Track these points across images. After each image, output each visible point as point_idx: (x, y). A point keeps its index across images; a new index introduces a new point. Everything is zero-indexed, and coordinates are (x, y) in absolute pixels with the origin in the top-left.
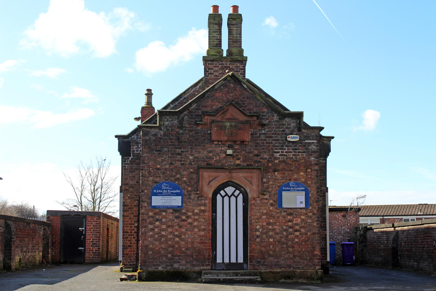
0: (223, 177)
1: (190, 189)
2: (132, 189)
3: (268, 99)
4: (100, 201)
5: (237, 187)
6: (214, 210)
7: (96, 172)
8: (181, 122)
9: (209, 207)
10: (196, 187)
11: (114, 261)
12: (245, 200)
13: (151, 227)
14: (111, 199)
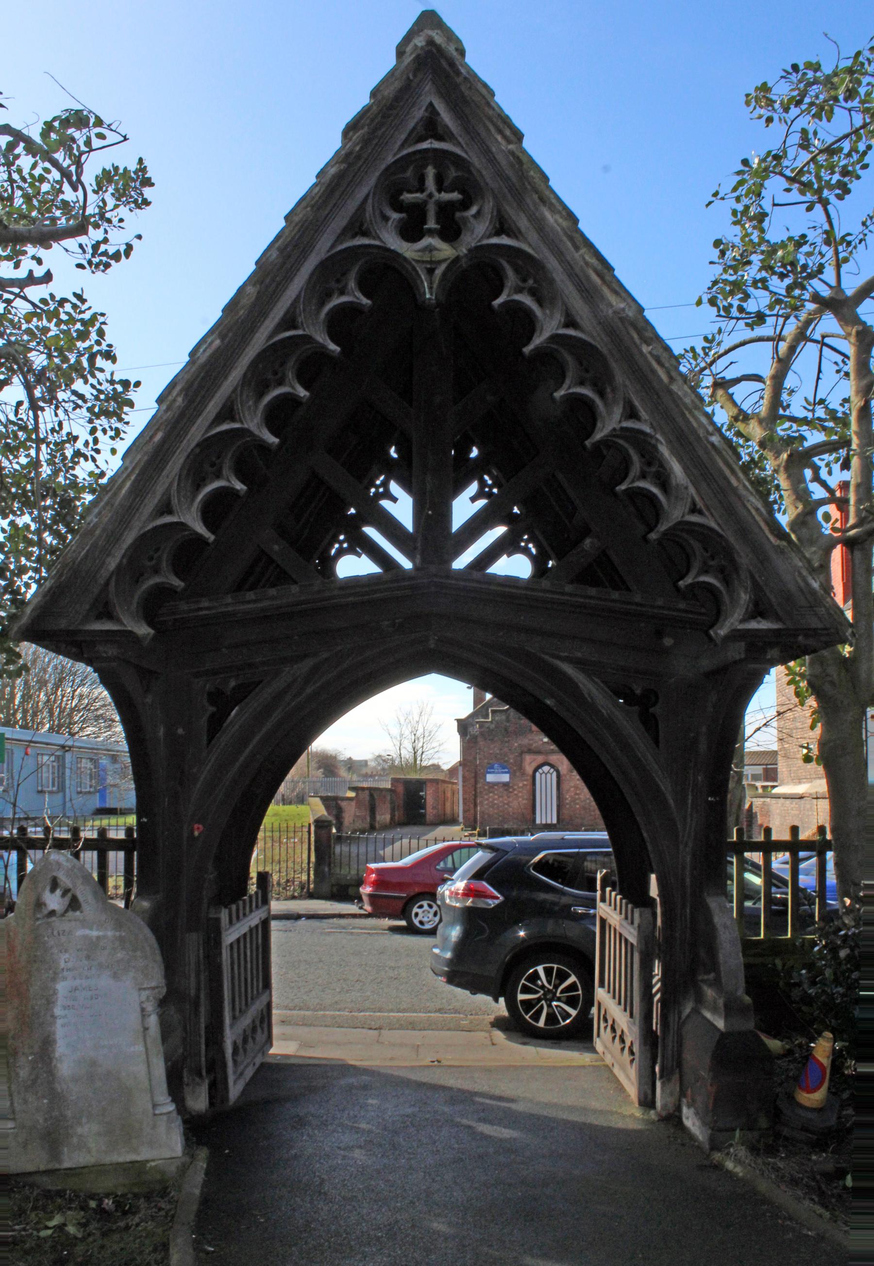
0: (540, 759)
1: (516, 769)
2: (471, 764)
6: (534, 784)
7: (416, 718)
9: (527, 783)
10: (520, 766)
11: (453, 821)
12: (559, 776)
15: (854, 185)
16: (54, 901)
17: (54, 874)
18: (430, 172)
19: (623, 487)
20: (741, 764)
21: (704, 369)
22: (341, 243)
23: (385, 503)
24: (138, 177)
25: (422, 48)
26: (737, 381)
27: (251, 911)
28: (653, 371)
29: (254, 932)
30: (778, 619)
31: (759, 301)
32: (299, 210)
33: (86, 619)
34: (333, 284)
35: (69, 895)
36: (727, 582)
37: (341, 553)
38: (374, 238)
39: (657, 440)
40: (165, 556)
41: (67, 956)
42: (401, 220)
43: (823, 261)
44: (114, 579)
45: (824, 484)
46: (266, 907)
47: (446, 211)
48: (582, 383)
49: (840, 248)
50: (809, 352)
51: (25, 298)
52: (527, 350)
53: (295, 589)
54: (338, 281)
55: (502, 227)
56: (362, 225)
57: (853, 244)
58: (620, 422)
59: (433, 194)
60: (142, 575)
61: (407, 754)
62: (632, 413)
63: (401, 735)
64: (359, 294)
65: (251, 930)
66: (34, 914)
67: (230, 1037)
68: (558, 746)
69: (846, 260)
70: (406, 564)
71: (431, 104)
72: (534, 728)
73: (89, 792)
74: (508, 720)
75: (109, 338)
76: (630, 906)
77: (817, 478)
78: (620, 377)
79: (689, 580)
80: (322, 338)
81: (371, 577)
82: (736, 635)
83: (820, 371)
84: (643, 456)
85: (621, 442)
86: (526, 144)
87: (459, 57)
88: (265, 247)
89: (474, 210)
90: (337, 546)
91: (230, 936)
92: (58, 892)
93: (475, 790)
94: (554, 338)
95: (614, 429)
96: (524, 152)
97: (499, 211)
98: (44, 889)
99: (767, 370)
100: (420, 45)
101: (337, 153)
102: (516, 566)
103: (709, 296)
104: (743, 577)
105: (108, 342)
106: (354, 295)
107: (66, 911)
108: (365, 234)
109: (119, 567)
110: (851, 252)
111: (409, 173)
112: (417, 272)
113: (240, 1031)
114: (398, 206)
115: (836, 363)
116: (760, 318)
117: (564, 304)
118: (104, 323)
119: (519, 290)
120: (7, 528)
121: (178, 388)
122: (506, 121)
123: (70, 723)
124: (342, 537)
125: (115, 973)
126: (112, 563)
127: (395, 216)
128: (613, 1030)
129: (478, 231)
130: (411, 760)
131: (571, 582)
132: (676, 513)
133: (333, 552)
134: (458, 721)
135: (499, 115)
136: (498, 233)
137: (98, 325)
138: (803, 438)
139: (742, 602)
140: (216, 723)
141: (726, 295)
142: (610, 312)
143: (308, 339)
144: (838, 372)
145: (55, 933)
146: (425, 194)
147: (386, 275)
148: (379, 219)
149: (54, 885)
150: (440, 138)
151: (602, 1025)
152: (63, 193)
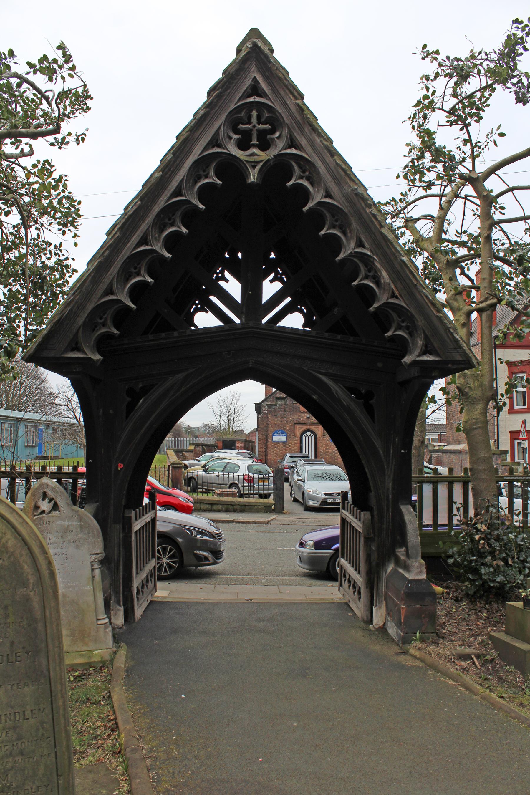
0: (305, 427)
1: (290, 434)
3: (406, 269)
4: (234, 423)
5: (312, 432)
8: (286, 402)
9: (298, 442)
10: (293, 431)
12: (316, 438)
13: (272, 450)
14: (242, 421)
15: (482, 114)
16: (45, 506)
17: (45, 490)
18: (254, 113)
19: (355, 283)
20: (423, 432)
21: (401, 211)
22: (206, 151)
23: (222, 283)
24: (84, 95)
25: (251, 48)
26: (419, 219)
27: (146, 513)
28: (372, 222)
29: (148, 525)
30: (438, 355)
31: (430, 176)
32: (184, 133)
33: (66, 351)
34: (201, 173)
35: (53, 502)
36: (411, 334)
37: (197, 310)
38: (224, 149)
39: (374, 258)
40: (109, 316)
41: (51, 536)
42: (238, 139)
43: (465, 156)
44: (81, 329)
45: (467, 276)
46: (154, 511)
47: (262, 134)
48: (334, 227)
49: (475, 150)
50: (458, 204)
51: (19, 165)
52: (305, 209)
53: (176, 334)
54: (204, 171)
55: (292, 143)
56: (217, 141)
57: (482, 147)
58: (354, 249)
59: (255, 125)
60: (96, 327)
61: (224, 423)
62: (360, 244)
63: (221, 412)
64: (216, 179)
65: (146, 524)
66: (33, 513)
67: (136, 583)
68: (319, 421)
69: (478, 156)
70: (237, 321)
71: (255, 77)
72: (302, 408)
73: (33, 447)
74: (286, 404)
75: (69, 189)
76: (358, 511)
77: (463, 273)
78: (355, 225)
79: (389, 334)
80: (195, 201)
81: (217, 327)
82: (415, 363)
83: (464, 215)
84: (366, 266)
85: (355, 259)
86: (305, 100)
87: (270, 54)
88: (166, 153)
89: (277, 134)
90: (194, 306)
91: (137, 526)
92: (47, 500)
93: (266, 446)
94: (320, 203)
95: (351, 253)
96: (304, 104)
97: (290, 135)
98: (39, 499)
99: (435, 212)
100: (249, 46)
101: (205, 103)
102: (295, 321)
103: (403, 174)
104: (419, 332)
105: (69, 191)
106: (213, 179)
107: (51, 511)
108: (219, 146)
109: (84, 322)
110: (480, 152)
111: (243, 114)
112: (247, 167)
113: (140, 581)
114: (236, 132)
115: (473, 210)
116: (431, 184)
117: (325, 185)
118: (66, 180)
119: (301, 178)
120: (7, 293)
121: (118, 227)
122: (295, 87)
123: (19, 404)
124: (197, 302)
125: (77, 545)
126: (80, 321)
127: (235, 137)
128: (349, 581)
129: (279, 147)
130: (227, 428)
131: (327, 332)
132: (383, 298)
133: (192, 310)
134: (256, 404)
135: (291, 85)
136: (290, 147)
137: (63, 181)
138: (454, 253)
139: (419, 345)
140: (131, 408)
141: (414, 171)
142: (349, 190)
143: (188, 202)
144: (474, 215)
145: (45, 523)
146: (251, 125)
147: (230, 168)
148: (227, 139)
149: (45, 496)
150: (259, 96)
151: (343, 579)
152: (42, 104)
